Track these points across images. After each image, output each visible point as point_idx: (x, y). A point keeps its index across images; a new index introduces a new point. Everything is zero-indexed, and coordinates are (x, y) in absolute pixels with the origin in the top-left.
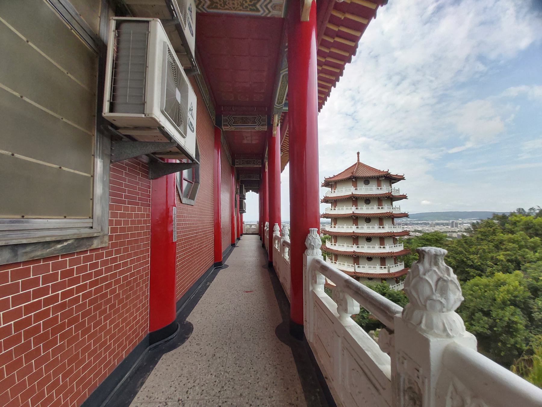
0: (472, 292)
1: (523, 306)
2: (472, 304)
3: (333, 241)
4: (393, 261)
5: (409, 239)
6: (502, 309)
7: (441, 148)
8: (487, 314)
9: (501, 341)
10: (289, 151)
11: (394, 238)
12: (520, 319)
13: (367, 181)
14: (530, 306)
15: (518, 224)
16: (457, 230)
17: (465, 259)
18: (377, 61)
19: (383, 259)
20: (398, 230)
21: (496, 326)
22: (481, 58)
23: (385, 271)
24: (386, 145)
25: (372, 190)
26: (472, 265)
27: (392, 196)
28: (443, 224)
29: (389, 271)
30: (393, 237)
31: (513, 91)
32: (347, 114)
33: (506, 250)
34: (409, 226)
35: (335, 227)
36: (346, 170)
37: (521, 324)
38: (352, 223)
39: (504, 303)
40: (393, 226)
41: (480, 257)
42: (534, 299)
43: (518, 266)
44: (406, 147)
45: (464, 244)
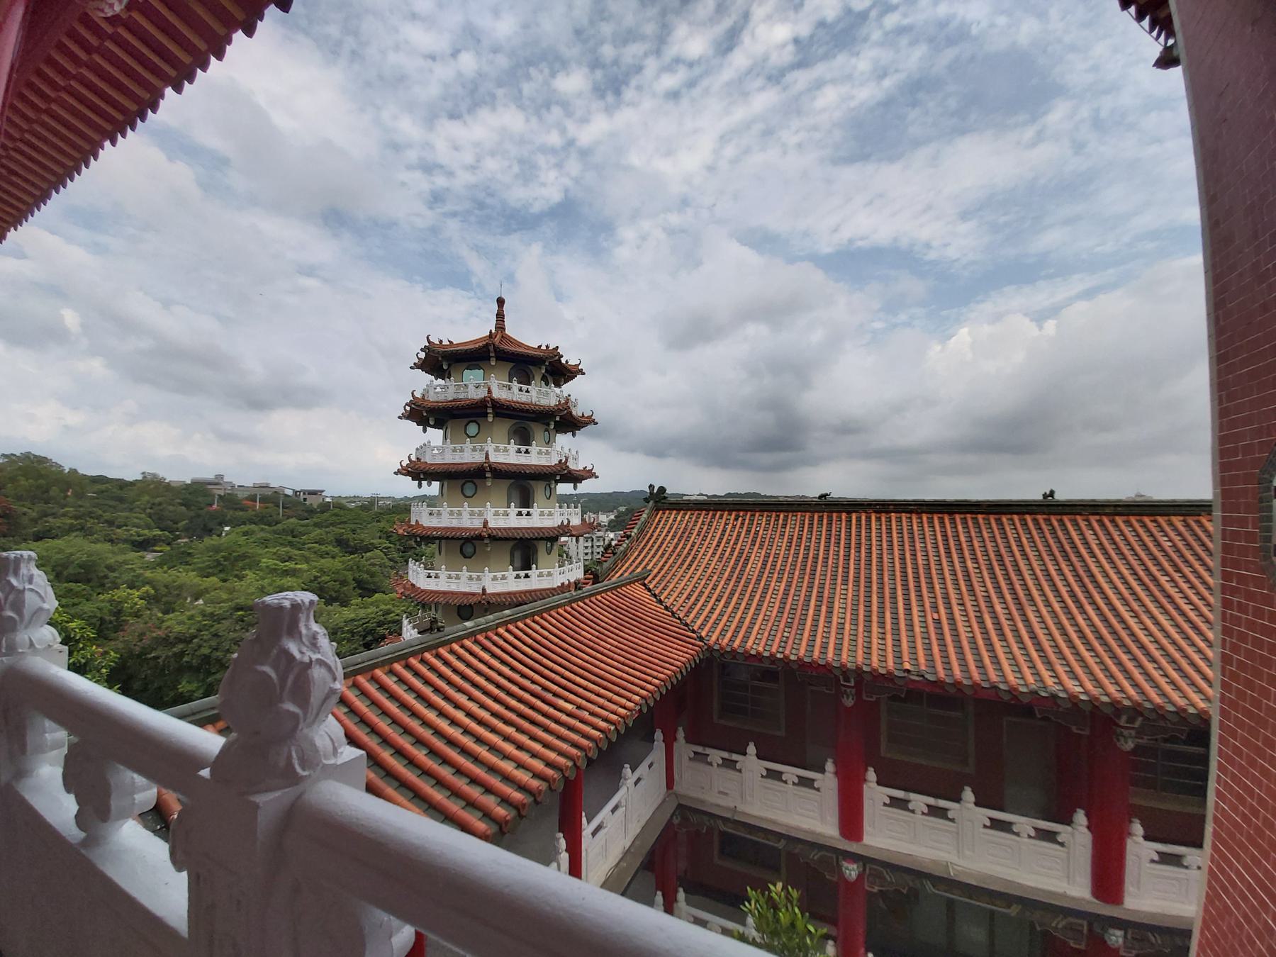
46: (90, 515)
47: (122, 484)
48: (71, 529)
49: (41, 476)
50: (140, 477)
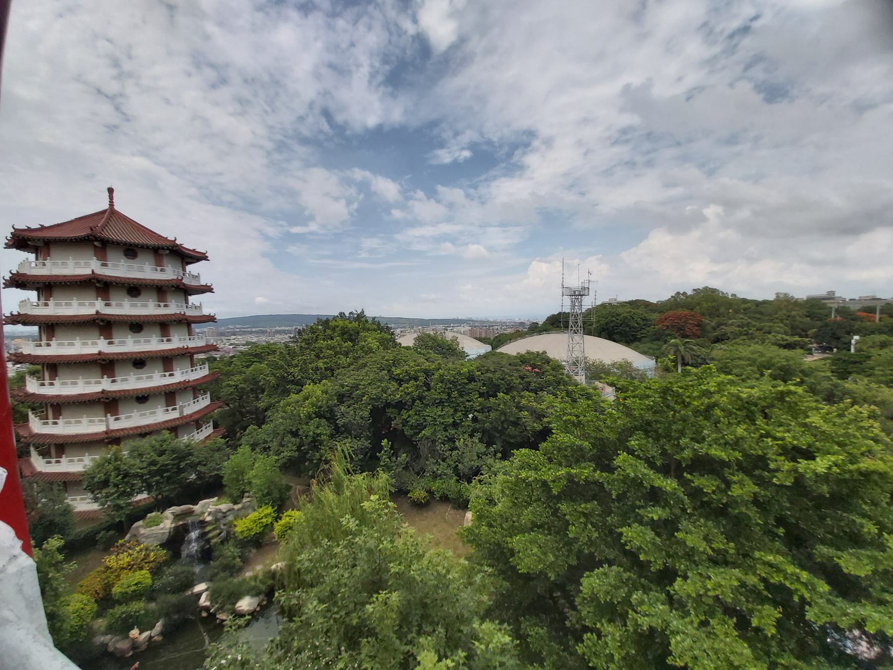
1: (329, 415)
3: (47, 375)
4: (191, 396)
6: (307, 424)
7: (280, 223)
8: (295, 434)
12: (325, 429)
13: (131, 251)
18: (172, 16)
19: (170, 395)
21: (303, 445)
22: (327, 114)
23: (175, 415)
24: (193, 191)
25: (144, 270)
27: (184, 285)
29: (181, 412)
30: (187, 355)
31: (359, 174)
32: (99, 92)
35: (48, 345)
36: (76, 219)
37: (324, 435)
38: (97, 333)
39: (310, 417)
41: (301, 370)
44: (230, 205)
46: (748, 324)
47: (757, 304)
48: (741, 334)
49: (714, 301)
50: (771, 297)
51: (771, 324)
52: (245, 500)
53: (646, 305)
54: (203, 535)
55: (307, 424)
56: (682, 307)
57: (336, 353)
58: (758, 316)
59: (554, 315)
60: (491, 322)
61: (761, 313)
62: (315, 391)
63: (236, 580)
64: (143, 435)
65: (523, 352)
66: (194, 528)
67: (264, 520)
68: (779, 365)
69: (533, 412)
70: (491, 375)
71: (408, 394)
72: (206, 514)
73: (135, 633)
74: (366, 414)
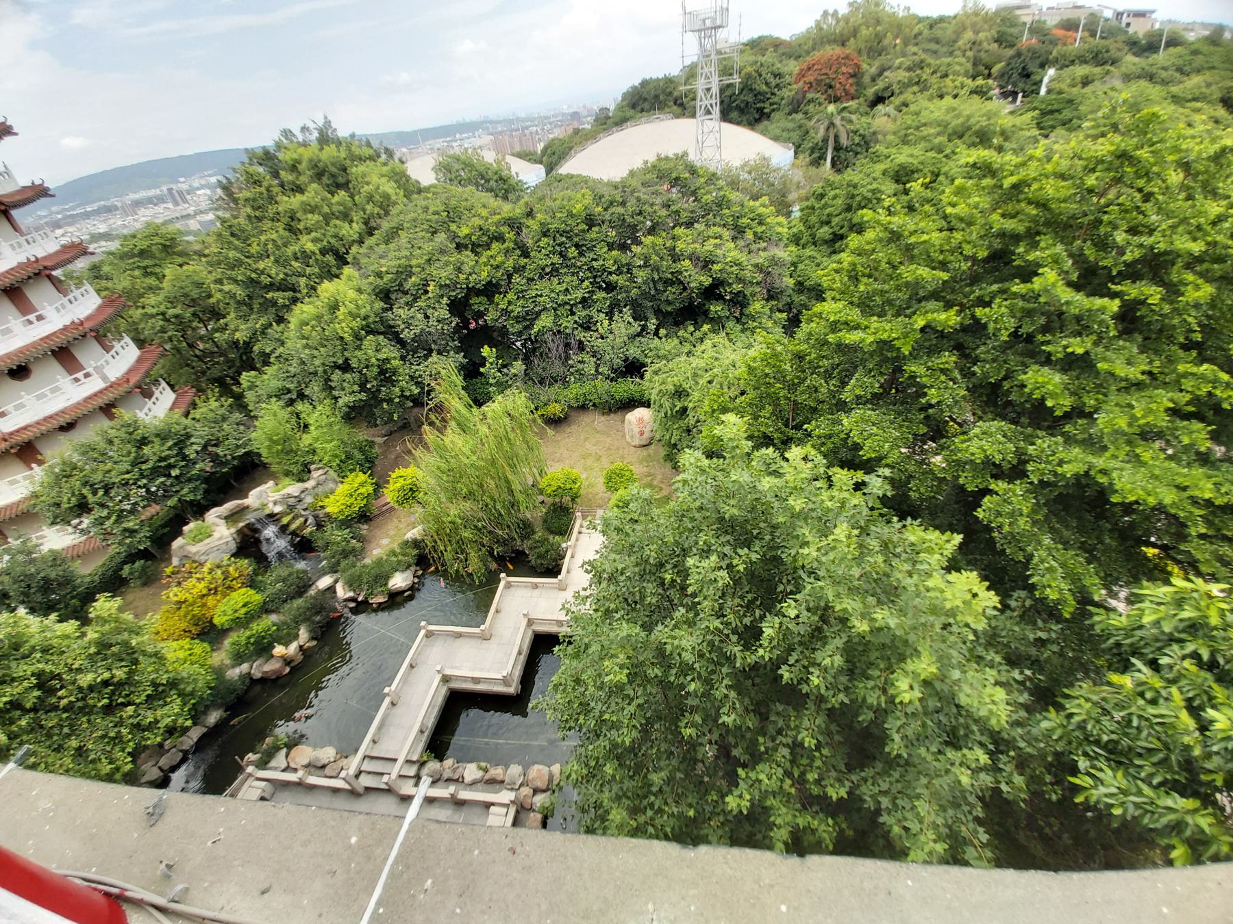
0: (304, 341)
2: (317, 362)
5: (95, 268)
6: (359, 348)
8: (346, 367)
9: (385, 400)
10: (980, 506)
11: (49, 277)
12: (390, 351)
14: (391, 323)
15: (300, 167)
16: (191, 210)
17: (253, 275)
19: (63, 353)
20: (45, 247)
23: (94, 385)
26: (272, 284)
28: (150, 201)
29: (104, 378)
33: (308, 231)
34: (70, 229)
37: (395, 358)
40: (22, 240)
41: (276, 261)
42: (391, 309)
43: (342, 260)
45: (232, 239)
46: (921, 65)
47: (933, 23)
48: (910, 84)
51: (949, 59)
52: (315, 474)
53: (777, 44)
54: (283, 529)
55: (359, 348)
56: (829, 42)
57: (327, 219)
58: (934, 46)
59: (634, 88)
60: (523, 120)
61: (937, 41)
62: (347, 291)
63: (368, 561)
64: (68, 427)
65: (652, 159)
66: (265, 526)
67: (363, 490)
68: (977, 127)
69: (694, 258)
70: (620, 210)
71: (498, 267)
72: (271, 505)
73: (279, 650)
74: (444, 313)
